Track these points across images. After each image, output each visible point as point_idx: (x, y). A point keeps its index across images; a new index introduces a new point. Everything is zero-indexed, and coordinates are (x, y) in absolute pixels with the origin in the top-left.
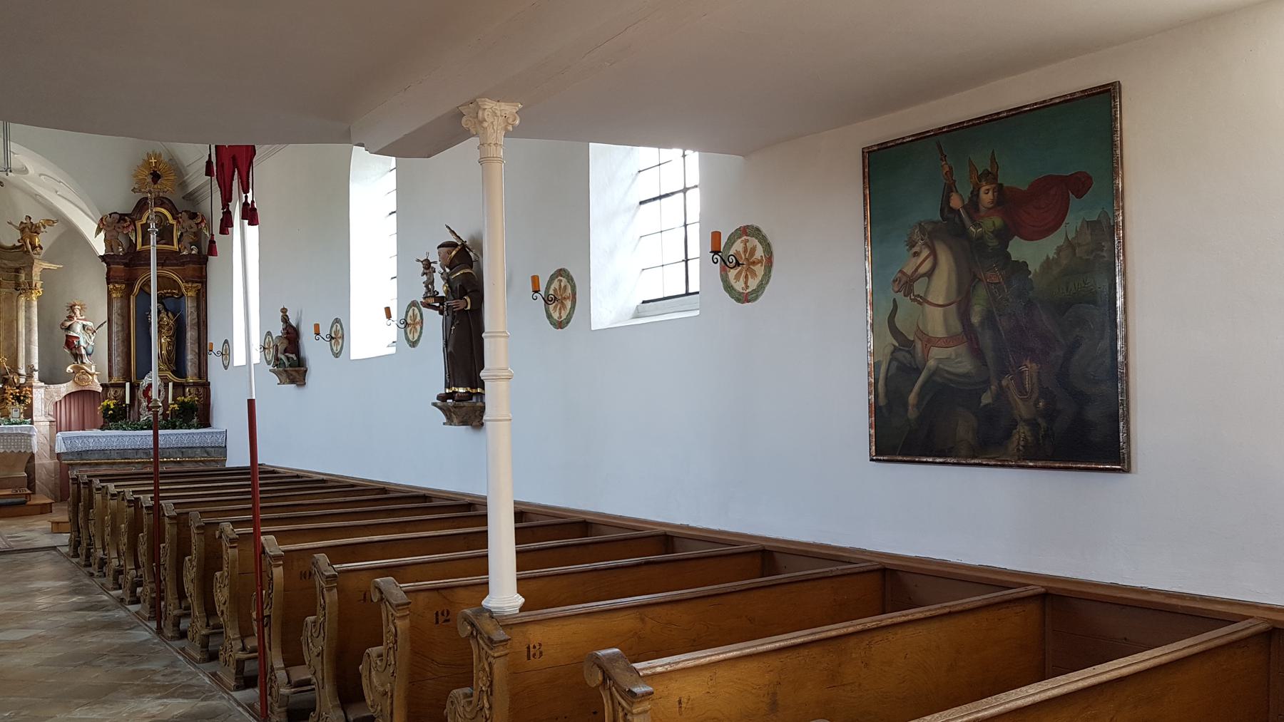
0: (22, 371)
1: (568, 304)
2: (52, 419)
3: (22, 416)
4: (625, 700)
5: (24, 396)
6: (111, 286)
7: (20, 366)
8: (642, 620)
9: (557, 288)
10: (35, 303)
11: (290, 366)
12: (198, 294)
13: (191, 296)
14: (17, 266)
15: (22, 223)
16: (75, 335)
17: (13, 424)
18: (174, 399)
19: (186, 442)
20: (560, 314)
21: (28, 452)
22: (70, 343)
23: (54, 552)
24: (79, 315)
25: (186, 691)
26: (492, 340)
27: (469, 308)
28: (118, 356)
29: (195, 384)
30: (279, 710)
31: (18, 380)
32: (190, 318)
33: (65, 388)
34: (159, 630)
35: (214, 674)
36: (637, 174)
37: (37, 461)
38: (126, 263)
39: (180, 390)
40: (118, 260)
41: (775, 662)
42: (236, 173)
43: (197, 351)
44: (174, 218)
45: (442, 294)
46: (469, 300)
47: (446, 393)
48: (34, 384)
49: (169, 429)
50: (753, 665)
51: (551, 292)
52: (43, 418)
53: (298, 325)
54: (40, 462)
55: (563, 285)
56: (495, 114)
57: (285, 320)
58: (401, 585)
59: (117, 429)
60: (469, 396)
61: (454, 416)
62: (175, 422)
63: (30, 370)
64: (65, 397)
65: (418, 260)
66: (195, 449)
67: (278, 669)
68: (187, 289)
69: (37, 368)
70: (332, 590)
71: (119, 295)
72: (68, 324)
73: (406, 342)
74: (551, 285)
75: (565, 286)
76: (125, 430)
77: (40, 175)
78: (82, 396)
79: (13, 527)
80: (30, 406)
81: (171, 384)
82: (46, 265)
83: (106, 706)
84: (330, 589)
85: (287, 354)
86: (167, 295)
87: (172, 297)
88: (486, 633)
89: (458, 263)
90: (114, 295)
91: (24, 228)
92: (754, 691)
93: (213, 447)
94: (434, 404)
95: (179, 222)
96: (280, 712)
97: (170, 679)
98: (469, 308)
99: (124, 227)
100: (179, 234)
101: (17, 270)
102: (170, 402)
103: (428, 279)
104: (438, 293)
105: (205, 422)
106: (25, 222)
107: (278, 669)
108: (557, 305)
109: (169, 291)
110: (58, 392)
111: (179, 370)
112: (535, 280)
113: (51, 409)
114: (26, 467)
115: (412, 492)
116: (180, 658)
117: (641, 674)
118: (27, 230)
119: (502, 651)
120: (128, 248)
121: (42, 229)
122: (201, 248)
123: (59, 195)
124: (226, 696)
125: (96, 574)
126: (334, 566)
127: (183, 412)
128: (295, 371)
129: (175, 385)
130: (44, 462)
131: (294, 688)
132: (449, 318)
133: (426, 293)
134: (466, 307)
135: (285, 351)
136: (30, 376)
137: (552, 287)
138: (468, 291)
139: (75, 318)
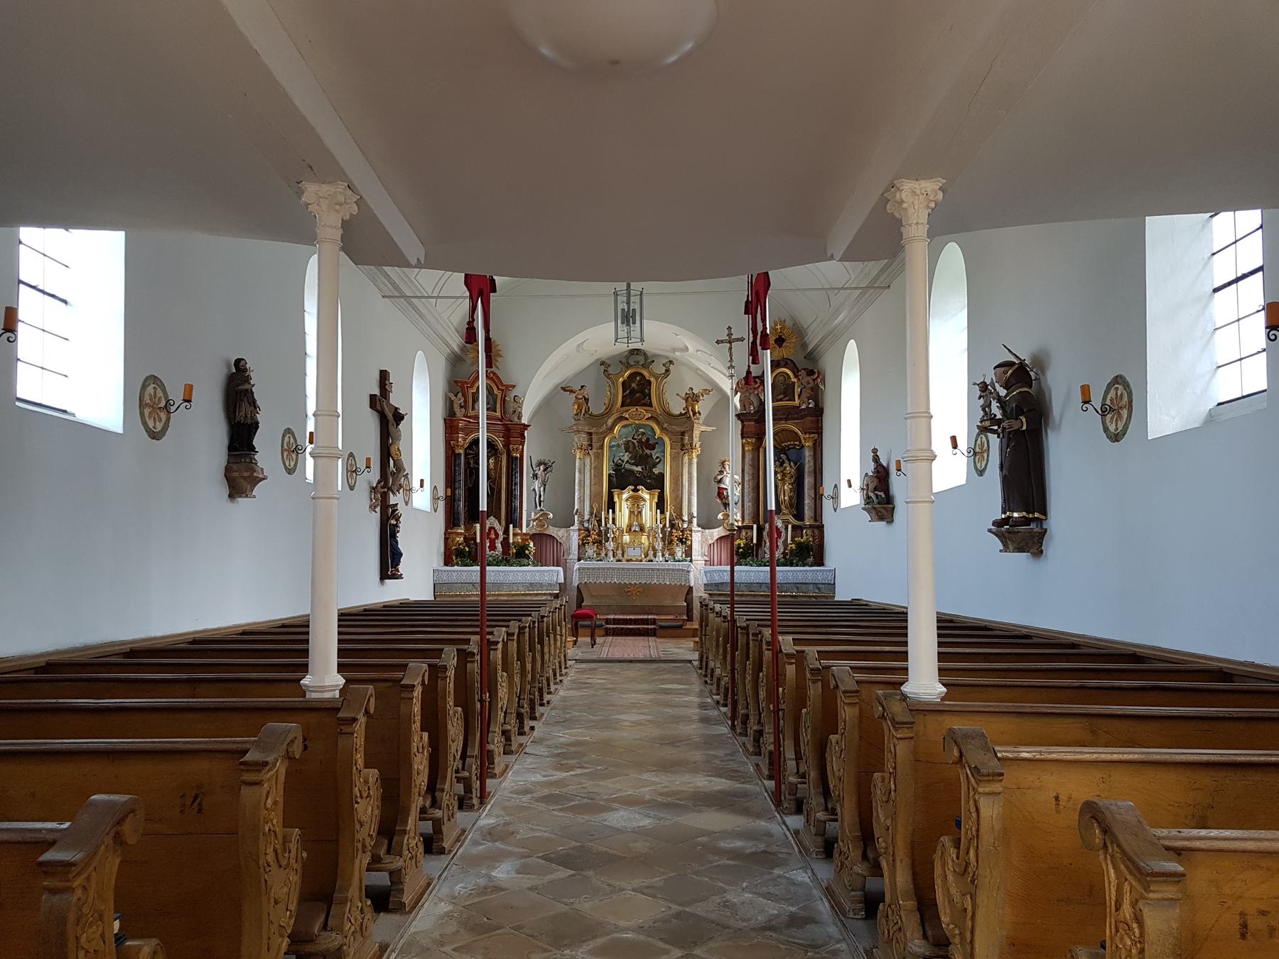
0: (686, 518)
1: (1125, 413)
2: (707, 559)
3: (684, 555)
4: (974, 778)
5: (686, 539)
6: (744, 441)
7: (684, 514)
8: (1093, 732)
9: (1114, 397)
10: (695, 460)
11: (879, 503)
12: (814, 444)
13: (809, 446)
14: (683, 430)
15: (686, 394)
16: (724, 487)
17: (677, 561)
18: (793, 539)
19: (801, 579)
20: (1116, 426)
21: (687, 585)
22: (721, 494)
23: (689, 665)
24: (728, 470)
25: (732, 775)
26: (913, 420)
27: (1024, 428)
28: (749, 501)
29: (811, 527)
30: (790, 797)
31: (682, 525)
32: (808, 465)
33: (717, 533)
34: (733, 727)
35: (757, 765)
36: (1209, 258)
37: (695, 594)
38: (756, 420)
39: (799, 532)
40: (750, 418)
41: (1207, 779)
42: (759, 308)
43: (813, 496)
44: (796, 376)
45: (999, 416)
46: (1024, 420)
47: (1002, 519)
48: (693, 529)
49: (787, 566)
50: (1171, 777)
51: (1108, 402)
52: (700, 558)
53: (888, 465)
54: (697, 595)
55: (1119, 393)
56: (914, 193)
57: (876, 459)
58: (855, 675)
59: (746, 565)
60: (1026, 521)
61: (1010, 543)
62: (792, 560)
63: (691, 516)
64: (717, 540)
65: (975, 384)
66: (808, 586)
67: (790, 759)
68: (805, 439)
69: (695, 515)
70: (816, 682)
71: (750, 448)
72: (719, 477)
73: (974, 471)
74: (1108, 394)
75: (1122, 394)
76: (752, 566)
77: (697, 351)
78: (729, 539)
79: (668, 644)
80: (690, 547)
81: (790, 526)
82: (703, 428)
83: (668, 774)
84: (815, 682)
85: (876, 492)
86: (790, 447)
87: (795, 448)
88: (891, 713)
89: (1014, 382)
90: (746, 449)
91: (688, 398)
92: (1170, 808)
93: (823, 584)
94: (990, 531)
95: (799, 379)
96: (790, 800)
97: (724, 763)
98: (1024, 428)
99: (755, 388)
100: (799, 390)
101: (683, 434)
102: (789, 542)
103: (985, 402)
104: (995, 416)
105: (820, 561)
106: (688, 392)
107: (790, 759)
108: (1113, 416)
109: (792, 443)
110: (712, 536)
111: (799, 516)
112: (1085, 390)
113: (706, 549)
114: (686, 598)
115: (970, 622)
116: (740, 750)
117: (999, 755)
118: (690, 399)
119: (907, 733)
120: (759, 407)
121: (701, 398)
122: (818, 402)
123: (712, 367)
124: (760, 783)
125: (709, 682)
126: (822, 661)
127: (799, 551)
128: (884, 508)
129: (794, 527)
130: (699, 593)
131: (801, 778)
132: (1005, 440)
133: (983, 416)
134: (1022, 427)
135: (875, 489)
136: (690, 522)
137: (1109, 398)
138: (1025, 410)
139: (725, 473)
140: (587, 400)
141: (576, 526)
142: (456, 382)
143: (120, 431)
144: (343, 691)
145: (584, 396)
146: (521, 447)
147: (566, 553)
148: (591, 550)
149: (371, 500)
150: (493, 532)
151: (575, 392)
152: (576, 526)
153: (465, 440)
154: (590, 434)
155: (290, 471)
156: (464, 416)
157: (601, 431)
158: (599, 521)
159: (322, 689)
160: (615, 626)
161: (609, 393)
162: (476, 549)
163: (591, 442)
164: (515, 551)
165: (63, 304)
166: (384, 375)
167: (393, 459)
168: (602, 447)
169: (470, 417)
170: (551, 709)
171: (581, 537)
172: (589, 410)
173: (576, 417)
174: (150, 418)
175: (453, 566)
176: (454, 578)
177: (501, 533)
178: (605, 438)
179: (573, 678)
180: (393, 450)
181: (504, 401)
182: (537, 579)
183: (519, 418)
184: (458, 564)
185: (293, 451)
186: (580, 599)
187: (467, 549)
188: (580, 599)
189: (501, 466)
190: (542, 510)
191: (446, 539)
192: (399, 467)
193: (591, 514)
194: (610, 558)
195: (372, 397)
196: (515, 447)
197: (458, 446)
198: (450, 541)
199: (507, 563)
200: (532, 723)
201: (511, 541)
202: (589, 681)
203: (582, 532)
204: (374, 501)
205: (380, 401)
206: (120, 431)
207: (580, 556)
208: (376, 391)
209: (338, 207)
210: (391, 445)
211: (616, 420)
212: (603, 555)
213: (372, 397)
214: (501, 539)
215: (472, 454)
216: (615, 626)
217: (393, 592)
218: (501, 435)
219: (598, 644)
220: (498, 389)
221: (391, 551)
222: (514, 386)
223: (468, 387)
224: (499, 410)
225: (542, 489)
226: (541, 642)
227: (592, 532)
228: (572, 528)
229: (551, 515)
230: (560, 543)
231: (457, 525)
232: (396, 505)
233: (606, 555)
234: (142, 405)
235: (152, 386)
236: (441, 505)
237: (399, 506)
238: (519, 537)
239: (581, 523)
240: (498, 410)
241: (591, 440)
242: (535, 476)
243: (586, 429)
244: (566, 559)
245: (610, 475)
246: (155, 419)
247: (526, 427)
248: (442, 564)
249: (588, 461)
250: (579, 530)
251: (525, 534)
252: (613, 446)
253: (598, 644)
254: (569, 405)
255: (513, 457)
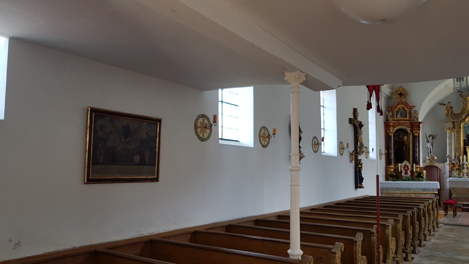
140: (452, 108)
141: (448, 162)
142: (389, 107)
143: (253, 146)
144: (302, 256)
145: (450, 106)
146: (418, 131)
147: (443, 174)
148: (455, 173)
149: (350, 158)
150: (406, 167)
151: (445, 105)
152: (448, 162)
153: (393, 130)
154: (454, 122)
155: (315, 152)
156: (393, 120)
157: (459, 120)
158: (459, 160)
159: (294, 255)
160: (467, 208)
161: (463, 104)
162: (399, 174)
163: (455, 126)
164: (416, 175)
165: (236, 106)
166: (355, 110)
167: (359, 142)
168: (460, 128)
169: (395, 121)
170: (426, 249)
171: (450, 167)
172: (453, 112)
173: (446, 115)
174: (263, 141)
175: (389, 180)
176: (389, 186)
177: (410, 167)
178: (461, 123)
179: (440, 233)
180: (359, 138)
181: (410, 113)
182: (427, 187)
183: (417, 119)
184: (391, 180)
185: (316, 145)
186: (451, 194)
187: (395, 174)
188: (451, 194)
189: (410, 139)
190: (431, 156)
191: (386, 170)
192: (362, 145)
193: (455, 157)
194: (465, 176)
195: (350, 120)
196: (416, 131)
197: (390, 132)
198: (388, 170)
199: (413, 180)
200: (413, 255)
201: (414, 170)
202: (448, 235)
203: (451, 165)
204: (351, 159)
205: (353, 120)
206: (253, 146)
207: (450, 175)
208: (352, 117)
209: (297, 80)
210: (358, 136)
211: (467, 115)
212: (461, 175)
213: (350, 120)
214: (410, 169)
215: (396, 135)
216: (467, 208)
217: (360, 193)
218: (409, 127)
219: (457, 216)
220: (408, 108)
221: (359, 177)
222: (414, 107)
223: (394, 109)
224: (408, 117)
225: (431, 147)
226: (419, 220)
227: (455, 165)
228: (446, 163)
229: (436, 158)
230: (441, 170)
231: (391, 164)
232: (361, 160)
233: (463, 175)
234: (260, 137)
235: (263, 130)
236: (384, 157)
237: (362, 160)
238: (418, 169)
239: (451, 161)
240: (408, 117)
241: (454, 125)
242: (428, 141)
243: (452, 120)
244: (444, 177)
245: (464, 140)
246: (264, 141)
247: (420, 123)
248: (384, 179)
249: (453, 134)
250: (449, 164)
251: (421, 168)
252: (465, 127)
253: (457, 216)
254: (443, 111)
255: (415, 136)
